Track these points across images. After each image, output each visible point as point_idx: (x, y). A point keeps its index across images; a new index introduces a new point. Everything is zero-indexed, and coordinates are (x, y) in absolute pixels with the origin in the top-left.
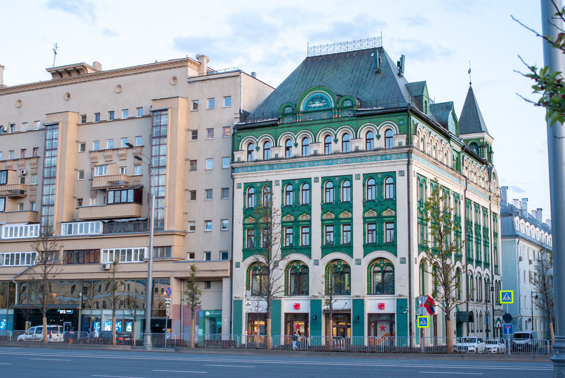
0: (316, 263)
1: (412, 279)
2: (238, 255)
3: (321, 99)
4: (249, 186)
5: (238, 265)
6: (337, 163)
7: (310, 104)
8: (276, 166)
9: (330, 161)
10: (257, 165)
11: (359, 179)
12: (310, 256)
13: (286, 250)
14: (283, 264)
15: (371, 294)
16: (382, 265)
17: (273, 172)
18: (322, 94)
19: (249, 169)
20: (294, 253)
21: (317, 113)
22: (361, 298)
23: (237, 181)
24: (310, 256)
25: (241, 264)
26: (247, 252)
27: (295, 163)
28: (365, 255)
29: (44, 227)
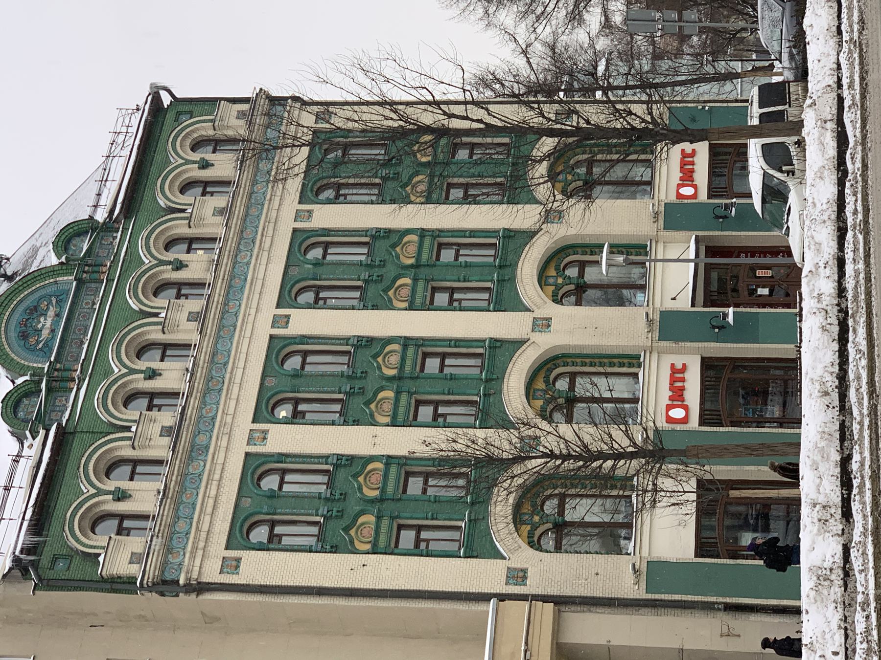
0: (543, 324)
1: (658, 394)
2: (484, 575)
3: (35, 311)
4: (239, 536)
5: (518, 576)
6: (248, 264)
7: (38, 342)
8: (201, 439)
9: (237, 282)
10: (180, 497)
11: (288, 317)
12: (530, 235)
13: (490, 414)
14: (523, 556)
15: (650, 183)
16: (560, 281)
17: (218, 443)
18: (21, 308)
19: (181, 525)
20: (500, 392)
21: (74, 322)
22: (662, 209)
23: (212, 573)
24: (518, 344)
25: (538, 314)
26: (477, 546)
27: (209, 379)
28: (499, 556)
29: (533, 12)
